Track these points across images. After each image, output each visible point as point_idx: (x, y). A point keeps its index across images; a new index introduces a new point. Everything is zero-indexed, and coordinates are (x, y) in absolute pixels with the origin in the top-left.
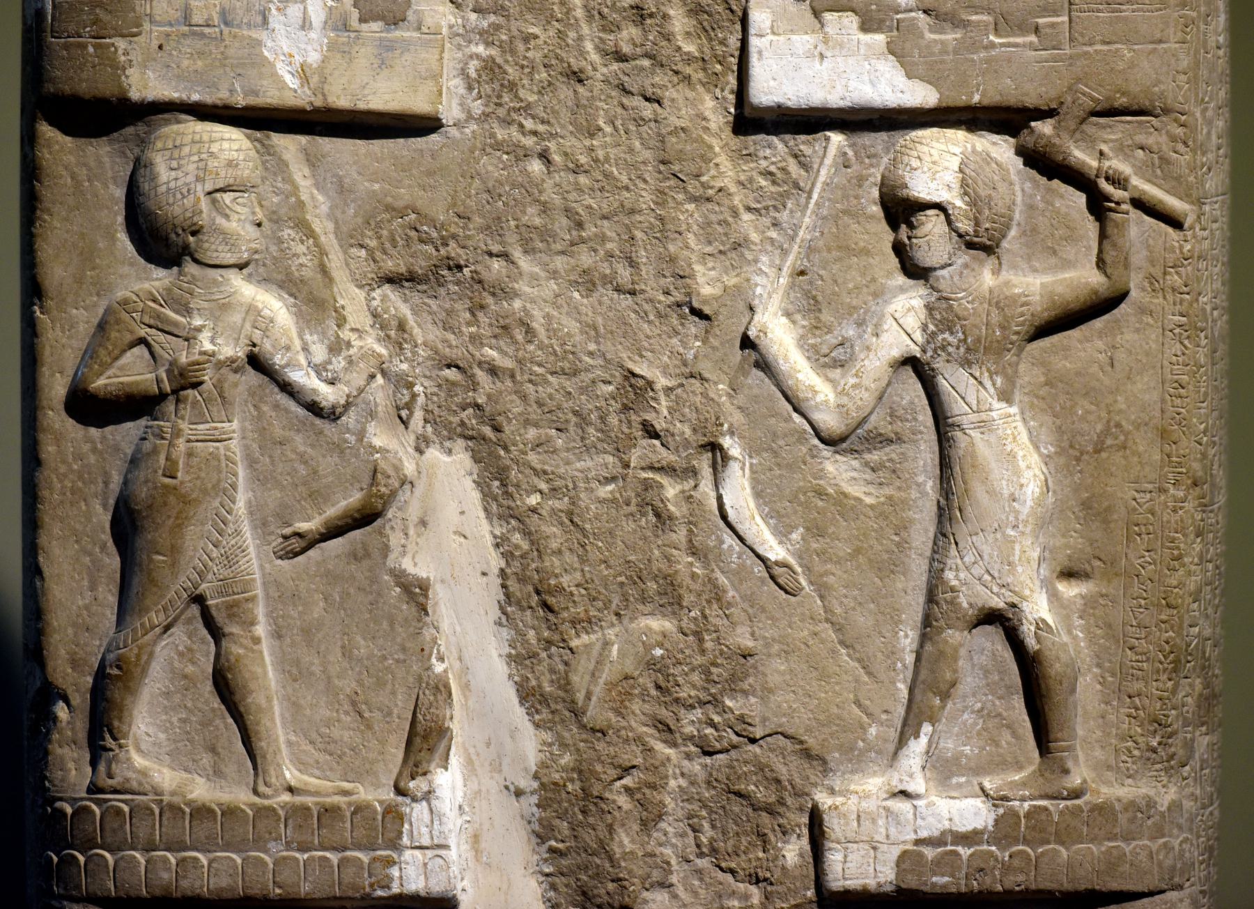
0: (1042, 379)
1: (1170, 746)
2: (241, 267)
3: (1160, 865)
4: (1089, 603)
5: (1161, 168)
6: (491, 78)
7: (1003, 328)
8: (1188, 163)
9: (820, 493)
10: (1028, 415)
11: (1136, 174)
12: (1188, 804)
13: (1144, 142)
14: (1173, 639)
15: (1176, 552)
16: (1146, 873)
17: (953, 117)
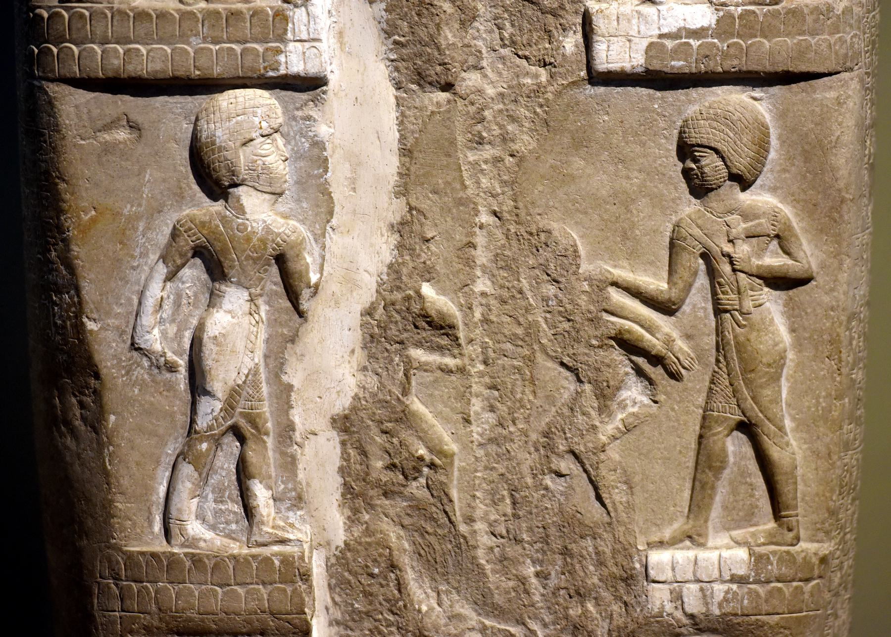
3: (836, 53)
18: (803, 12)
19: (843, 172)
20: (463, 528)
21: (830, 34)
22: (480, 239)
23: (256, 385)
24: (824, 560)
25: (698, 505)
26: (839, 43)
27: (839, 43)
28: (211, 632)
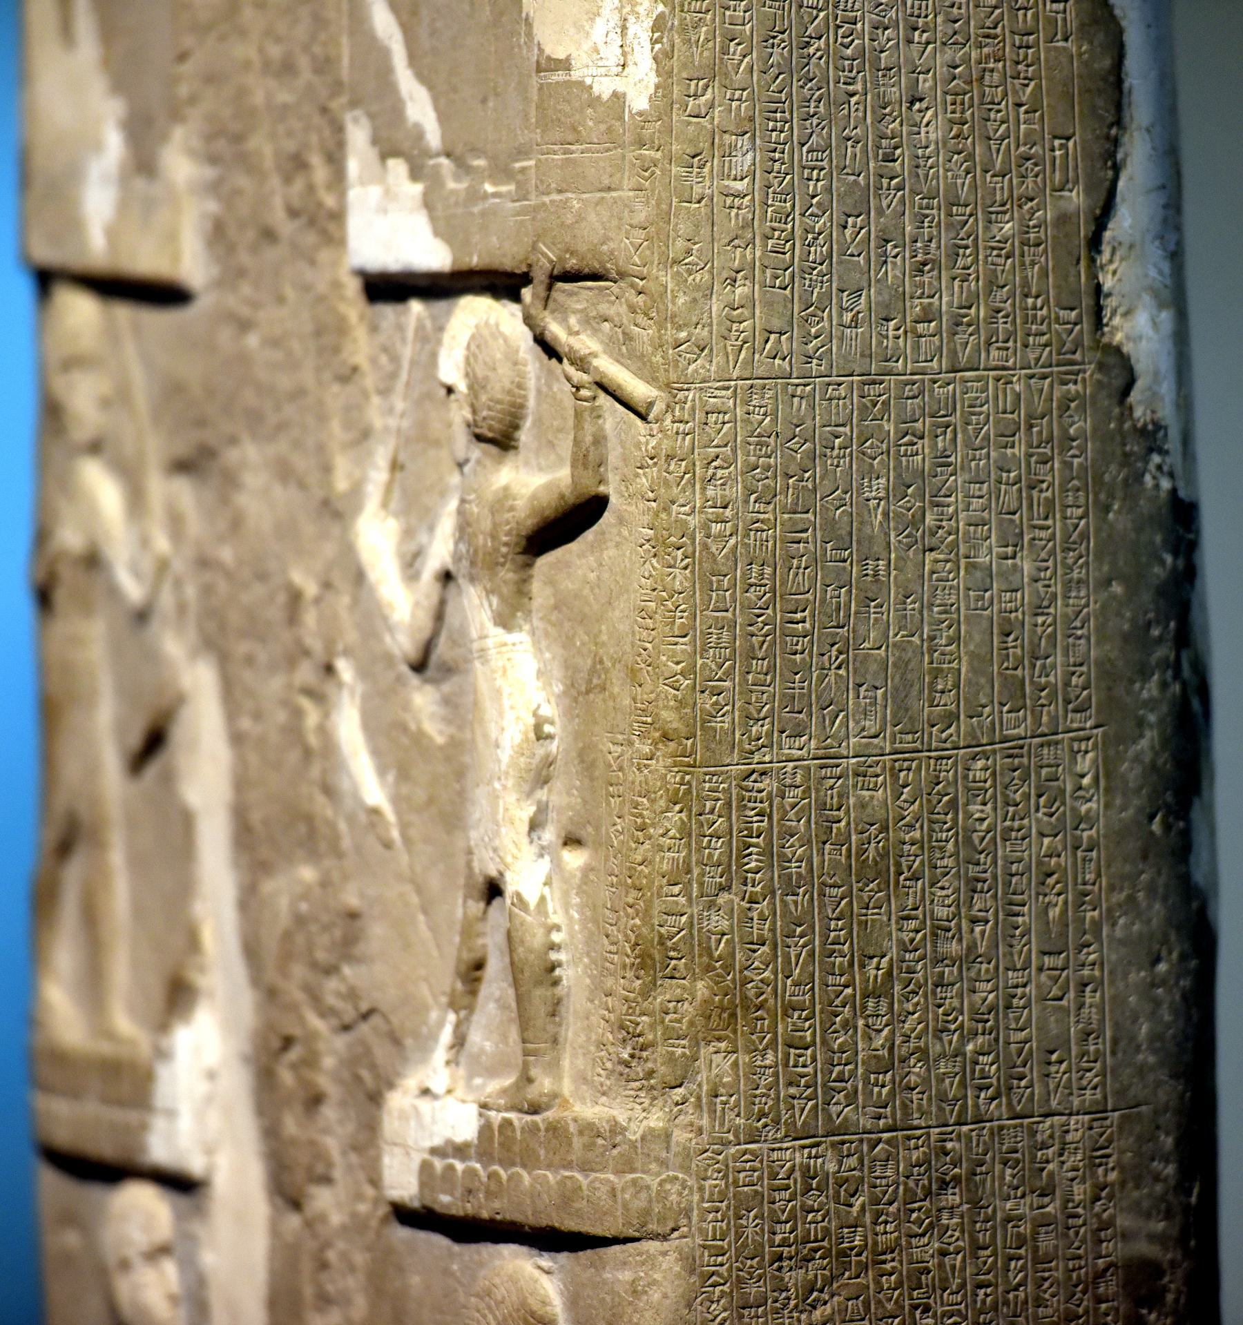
0: (552, 601)
1: (647, 1060)
3: (626, 1207)
4: (587, 870)
6: (218, 235)
7: (494, 537)
8: (651, 340)
9: (404, 728)
10: (544, 644)
11: (605, 352)
12: (680, 1136)
13: (607, 312)
14: (639, 927)
15: (639, 821)
16: (605, 1214)
17: (476, 281)
18: (567, 1130)
21: (617, 1172)
26: (631, 1190)
27: (631, 1190)
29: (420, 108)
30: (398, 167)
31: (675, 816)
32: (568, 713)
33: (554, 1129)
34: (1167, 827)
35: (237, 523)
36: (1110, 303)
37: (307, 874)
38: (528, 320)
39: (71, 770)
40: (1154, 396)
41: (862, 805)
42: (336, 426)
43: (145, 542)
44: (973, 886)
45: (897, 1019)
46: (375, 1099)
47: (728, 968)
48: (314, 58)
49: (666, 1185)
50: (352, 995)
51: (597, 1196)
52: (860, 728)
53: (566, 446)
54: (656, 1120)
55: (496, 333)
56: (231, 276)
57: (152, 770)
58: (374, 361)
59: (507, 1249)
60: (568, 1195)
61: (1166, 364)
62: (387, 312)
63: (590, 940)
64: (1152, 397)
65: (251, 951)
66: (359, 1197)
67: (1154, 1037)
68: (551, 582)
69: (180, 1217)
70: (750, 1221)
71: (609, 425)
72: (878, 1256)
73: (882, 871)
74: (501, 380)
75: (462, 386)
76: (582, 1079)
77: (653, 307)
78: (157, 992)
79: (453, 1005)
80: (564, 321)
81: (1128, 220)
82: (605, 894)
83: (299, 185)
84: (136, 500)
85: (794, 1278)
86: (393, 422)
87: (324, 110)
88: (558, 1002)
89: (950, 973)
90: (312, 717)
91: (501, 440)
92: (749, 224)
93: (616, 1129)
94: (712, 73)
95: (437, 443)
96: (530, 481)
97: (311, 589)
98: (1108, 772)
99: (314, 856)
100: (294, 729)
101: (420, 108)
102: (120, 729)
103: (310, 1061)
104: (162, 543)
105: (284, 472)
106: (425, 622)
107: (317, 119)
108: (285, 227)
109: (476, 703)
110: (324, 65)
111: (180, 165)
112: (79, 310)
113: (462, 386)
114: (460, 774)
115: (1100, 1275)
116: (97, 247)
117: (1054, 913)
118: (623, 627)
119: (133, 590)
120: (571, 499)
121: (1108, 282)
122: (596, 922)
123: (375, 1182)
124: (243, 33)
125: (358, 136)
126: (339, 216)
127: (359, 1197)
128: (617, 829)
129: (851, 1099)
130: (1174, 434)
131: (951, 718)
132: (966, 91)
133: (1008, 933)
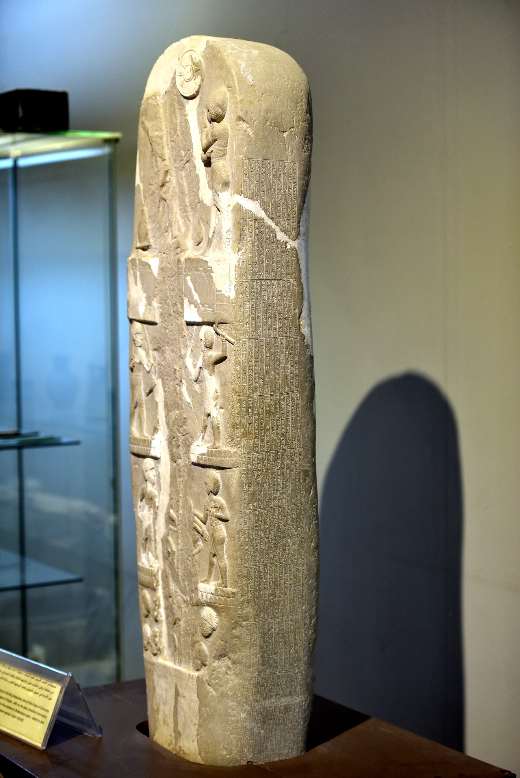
2: (140, 347)
4: (224, 413)
5: (230, 334)
6: (162, 315)
12: (239, 452)
19: (233, 494)
20: (177, 570)
22: (180, 500)
23: (150, 528)
24: (233, 593)
25: (210, 574)
28: (317, 595)
29: (196, 297)
30: (193, 306)
31: (238, 404)
32: (221, 389)
33: (219, 451)
34: (310, 405)
35: (165, 358)
36: (301, 327)
37: (177, 412)
38: (214, 330)
39: (137, 395)
40: (308, 340)
41: (266, 402)
42: (181, 344)
43: (149, 361)
44: (282, 414)
45: (271, 434)
46: (189, 446)
47: (246, 427)
48: (178, 289)
49: (237, 460)
50: (185, 430)
51: (226, 462)
52: (266, 391)
53: (221, 348)
54: (235, 450)
55: (209, 331)
56: (164, 321)
57: (150, 395)
58: (188, 335)
59: (211, 469)
60: (221, 461)
61: (309, 336)
62: (190, 327)
63: (224, 423)
64: (307, 341)
65: (168, 423)
66: (186, 461)
67: (308, 436)
68: (218, 369)
69: (156, 464)
70: (249, 465)
71: (227, 346)
72: (268, 470)
73: (268, 412)
74: (210, 339)
75: (203, 339)
76: (223, 444)
77: (235, 328)
78: (152, 430)
79: (202, 432)
80: (220, 330)
81: (304, 314)
82: (227, 416)
83: (175, 307)
84: (148, 354)
85: (256, 473)
86: (191, 344)
87: (180, 296)
88: (220, 432)
89: (278, 427)
90: (178, 388)
91: (210, 347)
92: (249, 315)
93: (229, 451)
94: (244, 293)
95: (199, 347)
96: (215, 354)
97: (178, 369)
98: (301, 397)
99: (178, 409)
100: (175, 390)
101: (196, 297)
102: (145, 389)
103: (178, 440)
104: (152, 361)
105: (173, 351)
106: (197, 374)
107: (178, 298)
108: (173, 314)
109: (206, 387)
110: (180, 290)
111: (155, 304)
112: (138, 326)
113: (203, 339)
114: (203, 397)
115: (300, 472)
116: (141, 317)
117: (293, 418)
118: (230, 376)
119: (148, 369)
120: (222, 357)
121: (301, 323)
122: (225, 419)
123: (189, 459)
124: (166, 284)
125: (186, 301)
126: (183, 313)
127: (186, 461)
128: (229, 406)
129: (264, 447)
130: (310, 346)
131: (279, 389)
132: (280, 294)
133: (287, 421)
